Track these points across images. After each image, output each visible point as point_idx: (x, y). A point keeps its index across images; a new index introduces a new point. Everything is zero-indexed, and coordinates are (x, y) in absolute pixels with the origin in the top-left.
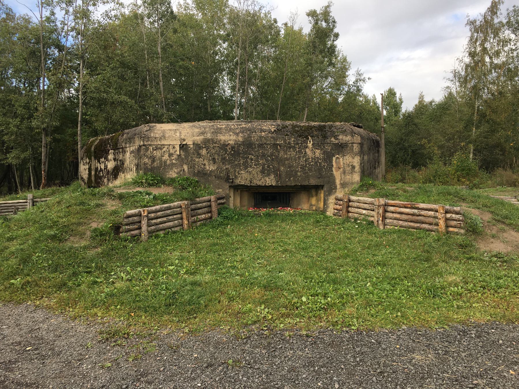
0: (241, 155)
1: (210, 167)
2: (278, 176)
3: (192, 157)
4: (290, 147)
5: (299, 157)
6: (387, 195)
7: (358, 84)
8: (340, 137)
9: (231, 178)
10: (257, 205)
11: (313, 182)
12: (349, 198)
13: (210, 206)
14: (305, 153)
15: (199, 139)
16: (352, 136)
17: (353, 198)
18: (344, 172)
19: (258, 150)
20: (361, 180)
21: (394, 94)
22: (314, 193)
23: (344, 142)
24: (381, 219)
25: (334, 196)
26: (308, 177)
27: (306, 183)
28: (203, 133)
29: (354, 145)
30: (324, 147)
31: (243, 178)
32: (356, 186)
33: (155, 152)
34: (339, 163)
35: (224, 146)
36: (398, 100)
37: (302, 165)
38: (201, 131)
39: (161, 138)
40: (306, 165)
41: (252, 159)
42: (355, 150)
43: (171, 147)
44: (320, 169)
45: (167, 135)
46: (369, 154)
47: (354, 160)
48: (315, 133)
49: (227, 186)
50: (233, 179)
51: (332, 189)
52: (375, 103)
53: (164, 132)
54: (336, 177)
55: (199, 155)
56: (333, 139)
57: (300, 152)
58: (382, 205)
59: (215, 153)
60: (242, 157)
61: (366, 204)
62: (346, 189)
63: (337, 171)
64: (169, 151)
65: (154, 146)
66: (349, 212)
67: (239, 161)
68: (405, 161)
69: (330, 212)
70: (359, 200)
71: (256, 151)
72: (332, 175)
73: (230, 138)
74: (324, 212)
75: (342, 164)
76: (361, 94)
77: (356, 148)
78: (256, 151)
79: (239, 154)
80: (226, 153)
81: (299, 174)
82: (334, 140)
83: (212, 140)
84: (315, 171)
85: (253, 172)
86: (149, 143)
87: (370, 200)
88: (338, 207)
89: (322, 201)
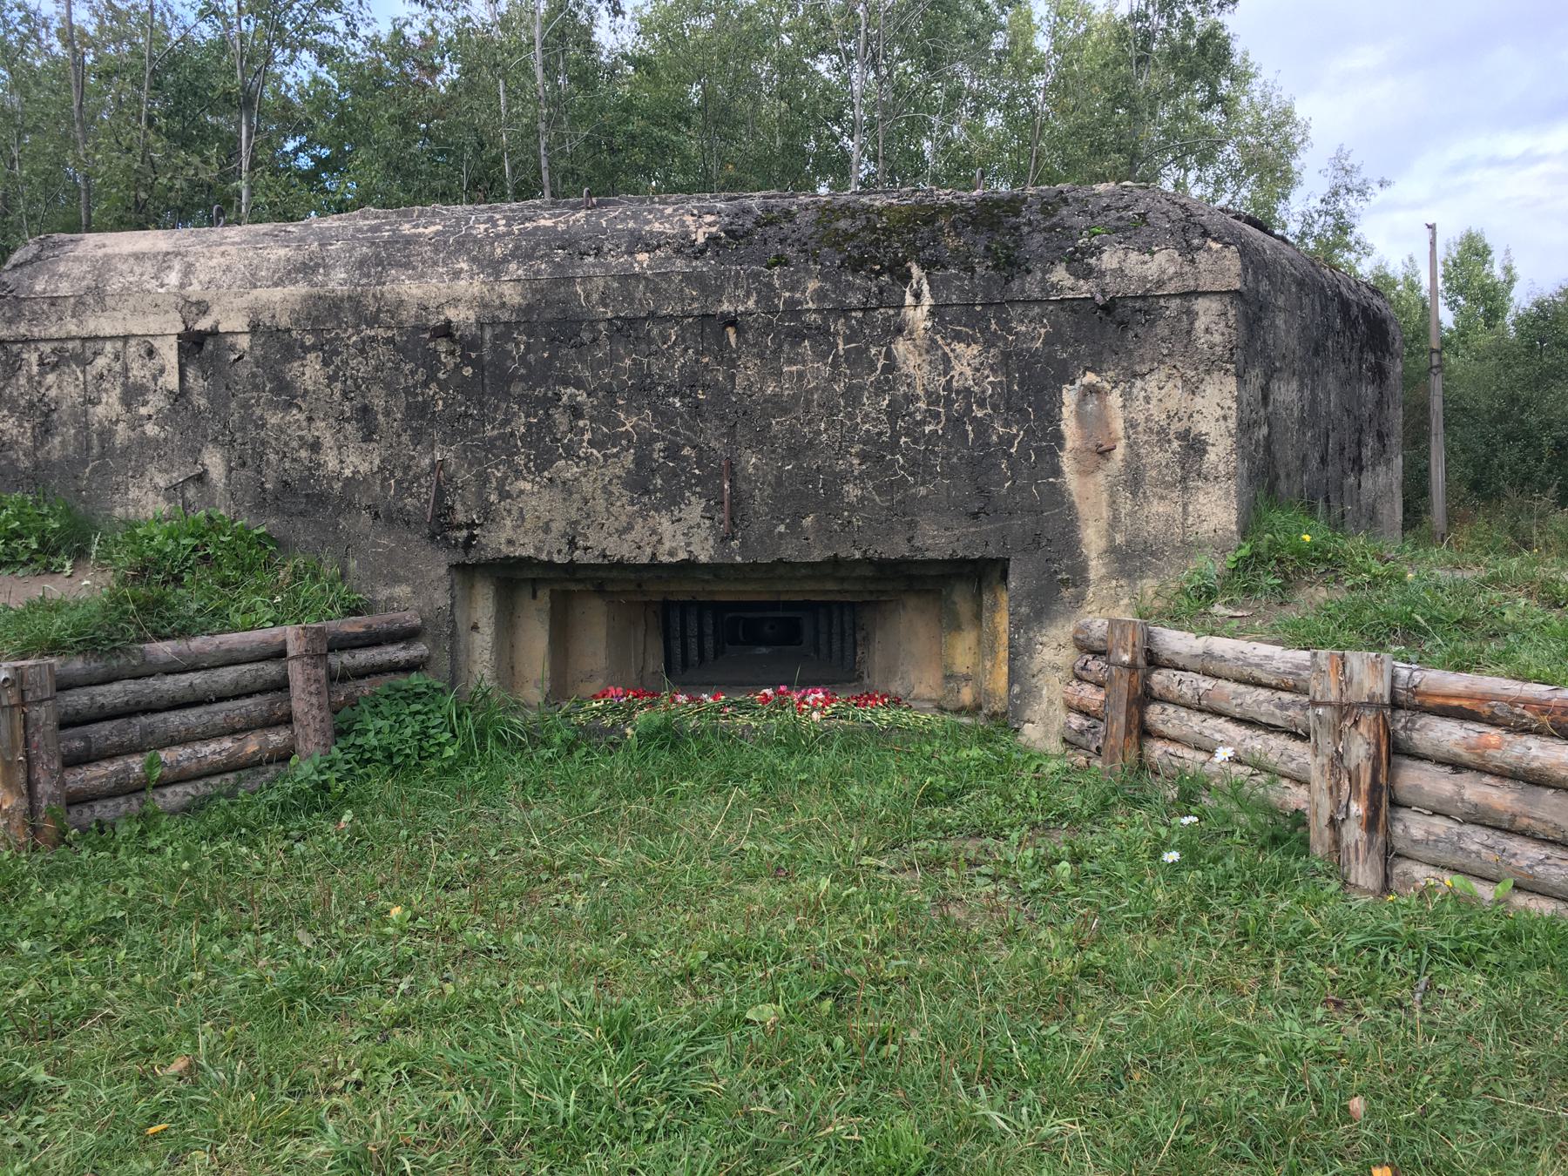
0: (517, 389)
1: (346, 460)
2: (732, 512)
3: (245, 405)
4: (792, 330)
5: (849, 388)
6: (1417, 627)
7: (1341, 206)
8: (1109, 260)
9: (461, 517)
10: (683, 668)
11: (937, 539)
12: (1150, 637)
13: (281, 686)
14: (891, 366)
15: (281, 299)
16: (1188, 250)
17: (1176, 641)
18: (1134, 479)
19: (613, 357)
20: (1248, 526)
22: (964, 608)
23: (1134, 288)
24: (1358, 808)
25: (1070, 628)
26: (905, 513)
27: (896, 548)
28: (306, 269)
29: (1200, 304)
30: (1005, 324)
31: (530, 518)
32: (1211, 566)
33: (51, 378)
34: (1103, 420)
37: (868, 439)
38: (300, 257)
39: (80, 302)
40: (895, 437)
41: (576, 411)
42: (1202, 341)
43: (133, 348)
44: (980, 465)
45: (115, 285)
46: (1309, 375)
47: (1199, 402)
48: (951, 242)
49: (436, 565)
50: (471, 525)
51: (1059, 583)
52: (1413, 287)
53: (103, 267)
54: (1083, 509)
55: (286, 393)
56: (1060, 275)
57: (858, 359)
58: (1370, 704)
59: (371, 380)
60: (522, 400)
61: (1258, 684)
62: (1149, 585)
63: (1085, 473)
64: (126, 369)
65: (47, 348)
66: (1146, 732)
67: (506, 422)
68: (1527, 478)
69: (1041, 731)
70: (1208, 654)
71: (601, 364)
72: (1057, 497)
73: (451, 291)
74: (1007, 721)
75: (1118, 426)
76: (1350, 239)
77: (1212, 323)
78: (601, 364)
79: (503, 380)
80: (431, 377)
81: (852, 492)
82: (1069, 281)
83: (355, 302)
84: (951, 472)
85: (587, 486)
86: (23, 329)
87: (1282, 658)
88: (1092, 696)
89: (1003, 654)
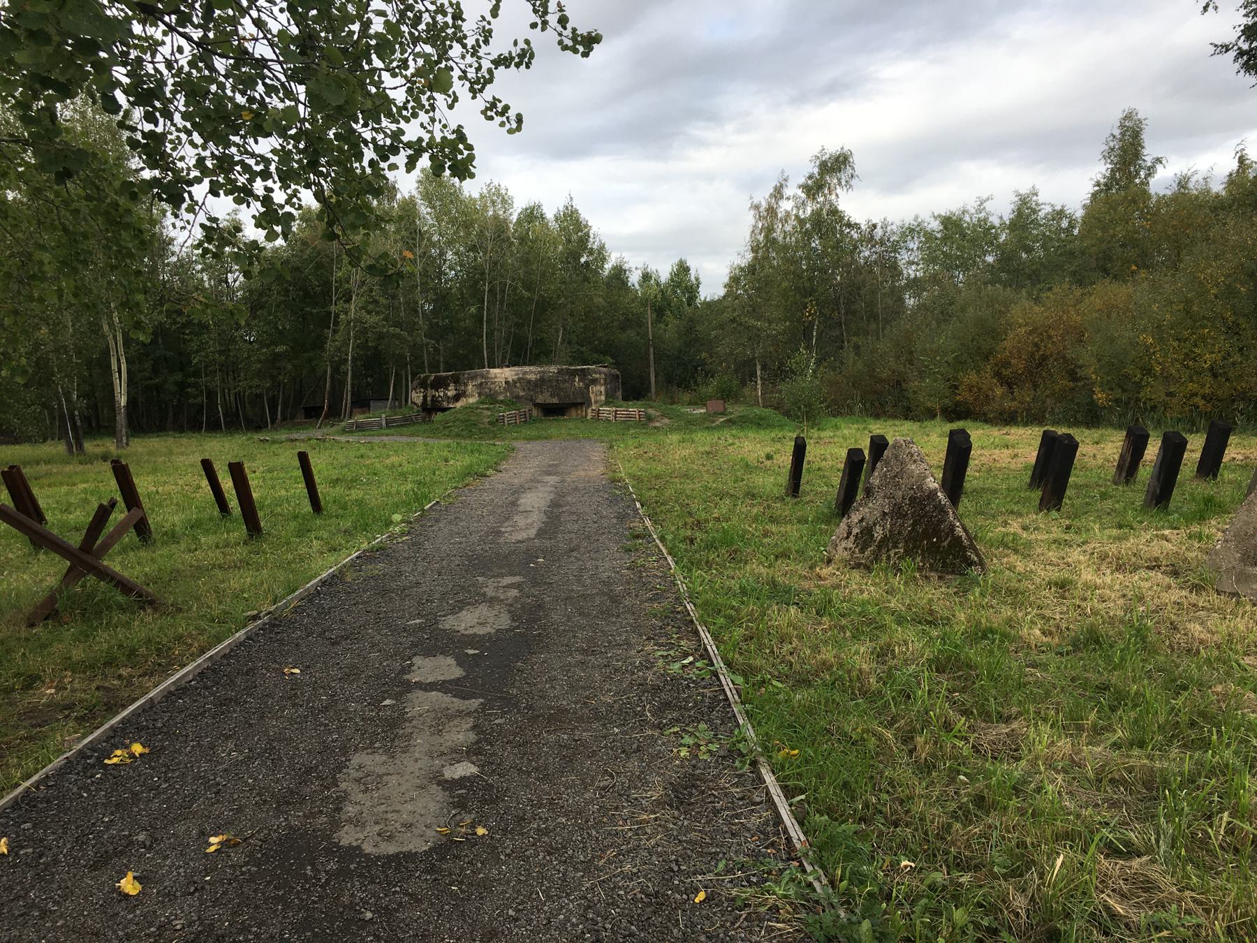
1: (522, 394)
2: (560, 398)
4: (565, 381)
11: (579, 401)
21: (687, 270)
35: (529, 381)
36: (693, 278)
51: (590, 404)
73: (532, 377)
